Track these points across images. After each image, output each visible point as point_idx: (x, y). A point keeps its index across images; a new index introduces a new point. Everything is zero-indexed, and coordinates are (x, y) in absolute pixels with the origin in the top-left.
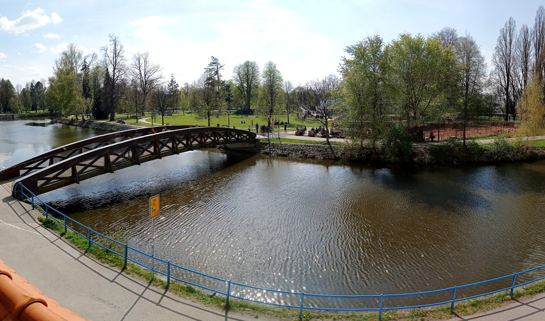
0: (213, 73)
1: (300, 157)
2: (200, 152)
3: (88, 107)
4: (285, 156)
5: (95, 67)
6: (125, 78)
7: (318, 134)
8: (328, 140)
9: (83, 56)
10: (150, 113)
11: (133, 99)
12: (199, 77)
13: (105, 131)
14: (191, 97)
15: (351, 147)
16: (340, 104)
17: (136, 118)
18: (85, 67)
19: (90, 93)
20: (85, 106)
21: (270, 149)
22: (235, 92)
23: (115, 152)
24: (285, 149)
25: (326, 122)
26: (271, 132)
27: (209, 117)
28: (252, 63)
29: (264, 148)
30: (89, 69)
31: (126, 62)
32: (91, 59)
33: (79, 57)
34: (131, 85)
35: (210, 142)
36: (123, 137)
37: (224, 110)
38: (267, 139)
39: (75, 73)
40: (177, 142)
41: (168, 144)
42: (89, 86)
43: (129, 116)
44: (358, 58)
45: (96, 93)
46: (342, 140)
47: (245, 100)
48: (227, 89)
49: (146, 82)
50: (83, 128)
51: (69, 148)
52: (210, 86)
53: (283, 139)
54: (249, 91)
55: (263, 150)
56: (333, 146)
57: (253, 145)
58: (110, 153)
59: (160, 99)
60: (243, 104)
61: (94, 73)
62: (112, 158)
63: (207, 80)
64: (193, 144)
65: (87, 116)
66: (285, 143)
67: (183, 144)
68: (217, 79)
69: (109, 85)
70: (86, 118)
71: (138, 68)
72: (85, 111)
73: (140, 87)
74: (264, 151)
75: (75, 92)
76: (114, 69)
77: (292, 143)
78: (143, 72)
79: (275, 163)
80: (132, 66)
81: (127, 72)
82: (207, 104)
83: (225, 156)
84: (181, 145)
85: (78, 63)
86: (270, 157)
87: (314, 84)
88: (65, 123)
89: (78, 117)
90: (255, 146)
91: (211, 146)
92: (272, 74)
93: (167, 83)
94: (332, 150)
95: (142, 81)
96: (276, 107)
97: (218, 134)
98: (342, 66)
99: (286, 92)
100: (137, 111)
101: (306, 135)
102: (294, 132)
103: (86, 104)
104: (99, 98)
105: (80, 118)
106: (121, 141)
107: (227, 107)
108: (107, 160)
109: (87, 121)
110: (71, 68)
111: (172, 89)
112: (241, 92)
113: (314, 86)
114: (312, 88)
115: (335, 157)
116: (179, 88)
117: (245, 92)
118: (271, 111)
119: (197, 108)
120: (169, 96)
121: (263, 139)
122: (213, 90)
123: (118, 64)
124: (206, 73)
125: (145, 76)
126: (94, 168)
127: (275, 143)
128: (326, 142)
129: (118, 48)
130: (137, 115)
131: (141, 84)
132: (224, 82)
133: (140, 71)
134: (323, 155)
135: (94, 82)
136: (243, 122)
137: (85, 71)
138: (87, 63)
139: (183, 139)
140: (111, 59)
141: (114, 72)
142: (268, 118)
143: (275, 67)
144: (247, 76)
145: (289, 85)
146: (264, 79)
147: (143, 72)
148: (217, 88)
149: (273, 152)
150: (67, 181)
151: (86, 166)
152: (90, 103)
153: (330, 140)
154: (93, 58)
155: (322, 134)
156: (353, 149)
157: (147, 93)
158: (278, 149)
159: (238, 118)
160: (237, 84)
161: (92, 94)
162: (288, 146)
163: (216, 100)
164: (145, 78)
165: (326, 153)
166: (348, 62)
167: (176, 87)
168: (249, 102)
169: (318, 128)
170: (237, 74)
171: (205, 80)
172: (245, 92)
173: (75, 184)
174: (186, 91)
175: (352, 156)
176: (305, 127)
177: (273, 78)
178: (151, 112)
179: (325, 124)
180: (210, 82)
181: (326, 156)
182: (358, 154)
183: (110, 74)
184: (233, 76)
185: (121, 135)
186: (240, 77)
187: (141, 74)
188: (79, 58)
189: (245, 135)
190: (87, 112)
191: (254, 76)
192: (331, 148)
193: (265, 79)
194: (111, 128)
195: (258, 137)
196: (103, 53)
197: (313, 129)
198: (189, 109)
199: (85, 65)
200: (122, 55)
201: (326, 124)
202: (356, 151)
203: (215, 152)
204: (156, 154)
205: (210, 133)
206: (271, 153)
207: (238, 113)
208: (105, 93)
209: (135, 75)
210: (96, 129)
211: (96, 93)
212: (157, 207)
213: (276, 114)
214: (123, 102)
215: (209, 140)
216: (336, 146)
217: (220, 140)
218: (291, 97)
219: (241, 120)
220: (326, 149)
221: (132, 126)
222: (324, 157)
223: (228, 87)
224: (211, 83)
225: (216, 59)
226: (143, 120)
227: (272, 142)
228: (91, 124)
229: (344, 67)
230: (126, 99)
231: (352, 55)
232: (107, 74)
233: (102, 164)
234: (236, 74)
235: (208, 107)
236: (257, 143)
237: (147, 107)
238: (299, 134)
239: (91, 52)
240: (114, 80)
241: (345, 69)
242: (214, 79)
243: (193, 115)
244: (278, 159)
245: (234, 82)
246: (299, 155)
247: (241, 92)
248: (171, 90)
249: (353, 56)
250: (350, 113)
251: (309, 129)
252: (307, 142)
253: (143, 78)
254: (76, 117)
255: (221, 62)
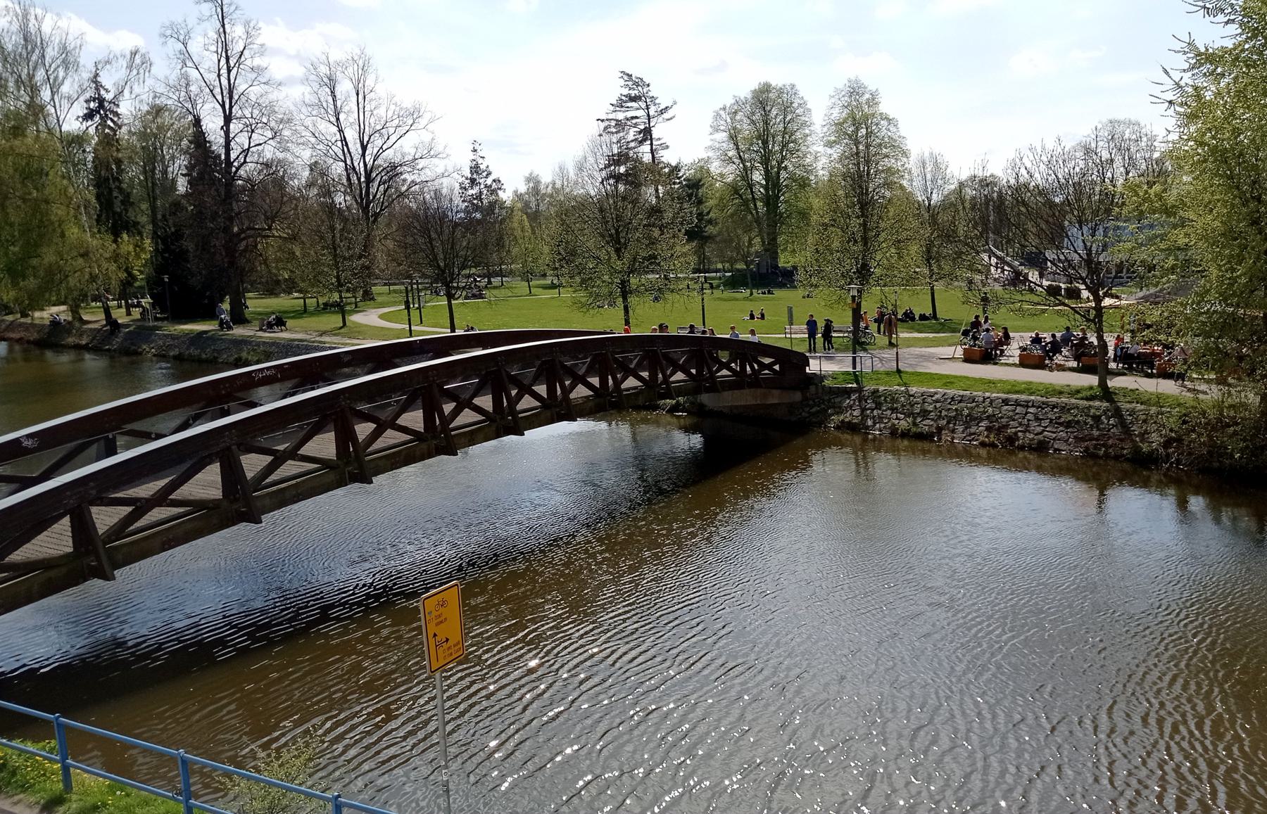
0: (631, 137)
1: (983, 444)
2: (603, 425)
3: (127, 270)
4: (921, 437)
5: (145, 108)
6: (281, 156)
7: (1058, 359)
8: (1103, 384)
9: (87, 63)
10: (395, 291)
11: (322, 238)
12: (581, 154)
13: (213, 365)
14: (555, 227)
15: (1212, 414)
16: (1163, 237)
17: (340, 308)
18: (100, 108)
19: (131, 214)
20: (113, 267)
21: (863, 410)
22: (722, 206)
23: (262, 441)
24: (925, 414)
25: (1099, 309)
26: (865, 350)
27: (625, 299)
28: (781, 92)
29: (840, 407)
30: (117, 114)
31: (276, 93)
32: (123, 73)
33: (66, 64)
34: (310, 185)
35: (635, 388)
36: (289, 384)
37: (683, 274)
38: (847, 373)
39: (50, 131)
40: (514, 392)
41: (477, 401)
42: (124, 186)
43: (311, 302)
44: (1255, 36)
45: (159, 217)
46: (1168, 387)
47: (760, 234)
48: (690, 196)
49: (368, 175)
50: (112, 358)
51: (47, 439)
52: (621, 187)
53: (913, 374)
54: (771, 201)
55: (838, 413)
56: (1128, 406)
57: (797, 396)
58: (239, 445)
59: (433, 235)
60: (753, 250)
61: (143, 135)
62: (252, 464)
63: (609, 166)
64: (572, 396)
65: (128, 307)
66: (924, 389)
67: (536, 396)
68: (647, 158)
69: (213, 181)
70: (120, 315)
71: (333, 119)
72: (115, 284)
73: (345, 193)
74: (842, 418)
75: (59, 212)
76: (228, 119)
77: (951, 392)
78: (351, 135)
79: (884, 465)
80: (304, 110)
81: (286, 133)
82: (618, 251)
83: (696, 440)
84: (527, 402)
85: (65, 89)
86: (865, 440)
87: (1044, 159)
88: (19, 341)
89: (81, 311)
90: (805, 399)
91: (640, 402)
92: (863, 131)
93: (455, 175)
94: (1122, 423)
95: (354, 168)
96: (883, 256)
97: (666, 356)
98: (1176, 76)
99: (920, 197)
100: (340, 285)
101: (1011, 361)
102: (959, 352)
103: (116, 257)
104: (178, 235)
105: (94, 316)
106: (284, 397)
107: (693, 260)
108: (232, 475)
109: (127, 326)
110: (29, 106)
111: (479, 196)
112: (746, 203)
113: (1043, 167)
114: (1037, 175)
115: (1137, 450)
116: (506, 196)
117: (759, 204)
118: (864, 273)
119: (581, 270)
120: (469, 225)
121: (834, 376)
122: (635, 202)
123: (243, 99)
124: (606, 138)
125: (364, 148)
126: (181, 510)
127: (881, 388)
128: (1098, 392)
129: (236, 32)
130: (341, 297)
131: (349, 179)
132: (676, 169)
133: (341, 131)
134: (1083, 440)
135: (149, 171)
136: (757, 314)
137: (103, 124)
138: (107, 91)
139: (536, 380)
140: (211, 77)
141: (227, 133)
142: (853, 297)
143: (873, 102)
144: (765, 143)
145: (936, 165)
146: (829, 151)
147: (351, 135)
148: (649, 194)
149: (875, 424)
150: (52, 574)
151: (142, 507)
152: (138, 256)
153: (1114, 383)
154: (130, 67)
155: (1077, 358)
156: (1220, 425)
157: (376, 215)
158: (893, 410)
159: (737, 300)
160: (731, 173)
161: (143, 219)
162: (937, 401)
163: (649, 238)
164: (363, 155)
165: (1096, 433)
166: (1206, 59)
167: (494, 192)
168: (775, 239)
169: (1058, 335)
170: (725, 134)
171: (603, 162)
172: (759, 204)
173: (97, 583)
174: (533, 205)
175: (1216, 451)
176: (1005, 329)
177: (868, 146)
178: (402, 288)
179: (1093, 321)
180: (622, 169)
181: (1095, 447)
182: (1247, 447)
183: (210, 138)
184: (710, 143)
185: (283, 373)
186: (738, 149)
187: (344, 140)
188: (67, 68)
189: (767, 361)
190: (126, 291)
191: (789, 141)
192: (1118, 413)
193: (836, 152)
194: (239, 352)
195: (814, 366)
196: (171, 54)
197: (1037, 340)
198: (550, 272)
199: (101, 101)
200: (257, 62)
201: (1097, 318)
202: (1235, 433)
203: (657, 423)
204: (434, 437)
205: (636, 356)
206: (867, 428)
207: (736, 282)
208: (199, 215)
209: (321, 147)
210: (175, 358)
211: (159, 217)
212: (453, 628)
213: (882, 282)
214: (280, 249)
215: (631, 382)
216: (1139, 407)
217: (672, 379)
218: (943, 218)
219: (750, 306)
220: (1097, 419)
221: (325, 339)
222: (1087, 449)
223: (695, 186)
224: (627, 174)
225: (639, 83)
226: (369, 318)
227: (869, 387)
228: (147, 340)
229: (1182, 83)
230: (294, 238)
231: (1227, 23)
232: (200, 139)
233: (216, 493)
234: (723, 136)
235: (618, 265)
236: (813, 388)
237: (382, 266)
238: (977, 356)
239: (125, 41)
240: (229, 163)
241: (1190, 90)
242: (638, 160)
243: (566, 294)
244: (895, 451)
245: (715, 167)
246: (981, 438)
247: (746, 203)
248: (475, 204)
249: (1234, 29)
250: (1214, 272)
251: (1020, 340)
252: (1014, 388)
253: (357, 157)
254: (75, 310)
255: (660, 91)
